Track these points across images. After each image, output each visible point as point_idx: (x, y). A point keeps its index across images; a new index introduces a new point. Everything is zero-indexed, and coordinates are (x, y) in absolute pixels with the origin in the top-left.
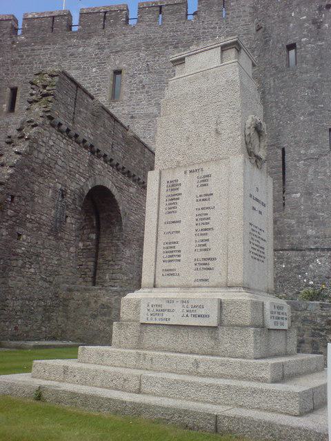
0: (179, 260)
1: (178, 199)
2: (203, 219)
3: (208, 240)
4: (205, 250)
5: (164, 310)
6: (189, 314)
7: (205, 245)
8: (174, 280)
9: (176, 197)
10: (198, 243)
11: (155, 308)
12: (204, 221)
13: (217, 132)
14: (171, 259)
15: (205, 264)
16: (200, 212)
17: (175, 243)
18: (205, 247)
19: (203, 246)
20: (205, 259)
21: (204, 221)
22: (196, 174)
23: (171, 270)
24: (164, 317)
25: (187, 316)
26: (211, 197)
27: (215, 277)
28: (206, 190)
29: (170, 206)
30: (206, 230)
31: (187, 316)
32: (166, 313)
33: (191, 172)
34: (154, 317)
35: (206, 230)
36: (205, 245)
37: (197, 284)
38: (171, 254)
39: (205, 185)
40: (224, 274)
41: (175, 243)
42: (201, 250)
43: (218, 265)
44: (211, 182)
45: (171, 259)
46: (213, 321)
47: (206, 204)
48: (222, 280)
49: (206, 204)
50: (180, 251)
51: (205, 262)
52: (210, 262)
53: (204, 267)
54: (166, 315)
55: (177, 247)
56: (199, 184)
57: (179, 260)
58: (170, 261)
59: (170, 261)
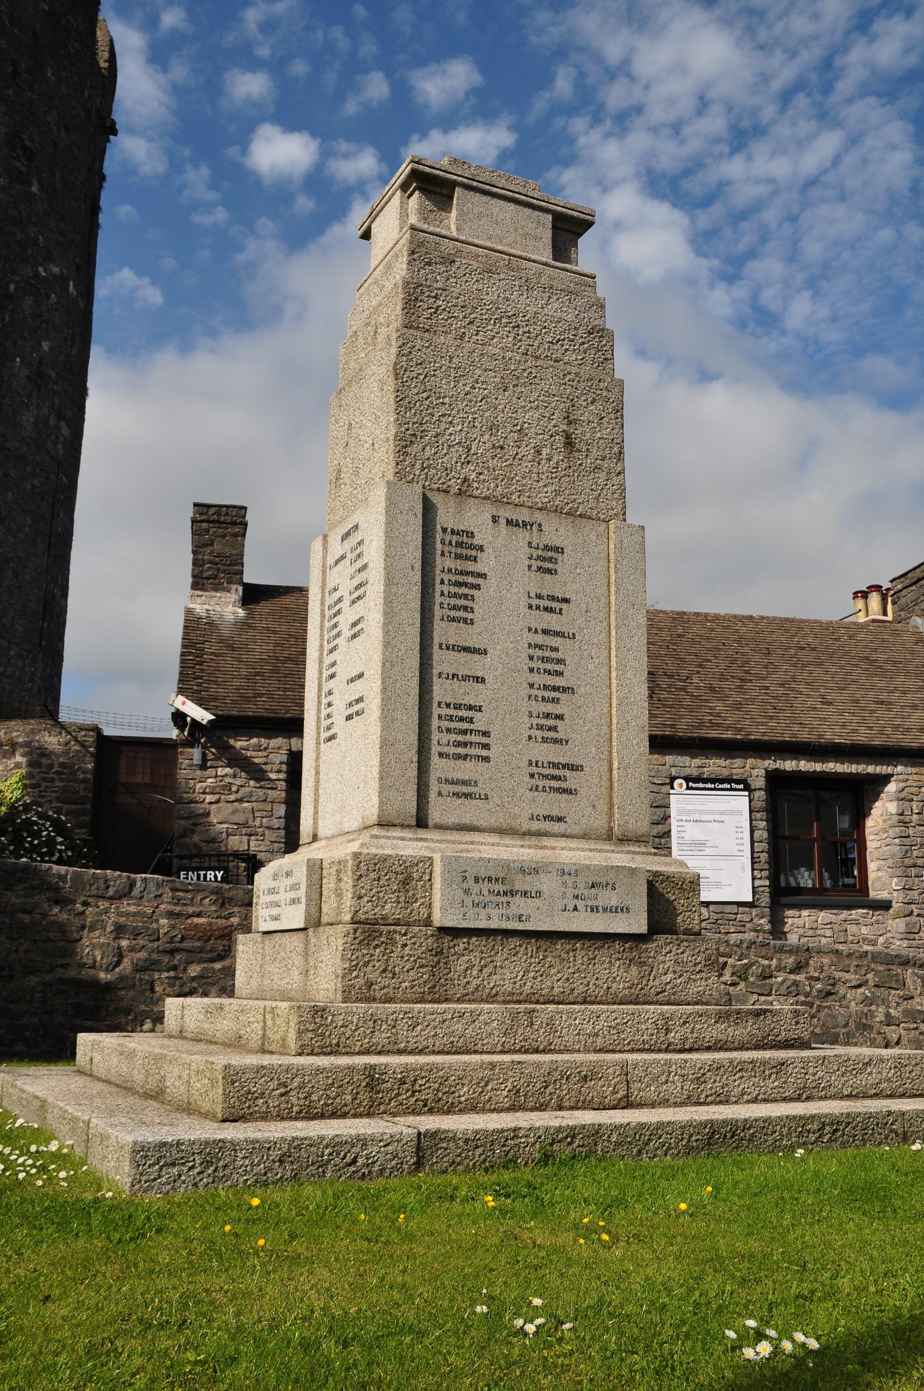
0: (486, 759)
1: (477, 587)
2: (546, 657)
3: (560, 717)
4: (556, 741)
5: (512, 893)
6: (580, 904)
7: (554, 729)
8: (469, 812)
9: (470, 580)
10: (535, 721)
11: (485, 887)
12: (549, 666)
13: (569, 443)
14: (460, 750)
15: (556, 777)
16: (540, 639)
17: (471, 708)
18: (552, 734)
19: (549, 728)
20: (556, 766)
21: (549, 666)
22: (523, 536)
23: (465, 783)
24: (514, 910)
25: (575, 909)
26: (564, 606)
27: (583, 812)
28: (551, 586)
29: (453, 601)
30: (555, 689)
31: (575, 909)
32: (517, 899)
33: (509, 522)
34: (483, 913)
35: (555, 689)
36: (554, 729)
37: (535, 826)
38: (460, 738)
39: (549, 571)
40: (602, 806)
41: (471, 708)
42: (545, 740)
43: (588, 784)
44: (564, 564)
45: (460, 750)
46: (638, 923)
47: (552, 621)
48: (599, 823)
49: (552, 621)
50: (486, 734)
51: (556, 772)
52: (568, 773)
53: (554, 784)
54: (519, 905)
55: (480, 721)
56: (535, 564)
57: (486, 759)
58: (458, 757)
59: (458, 757)
